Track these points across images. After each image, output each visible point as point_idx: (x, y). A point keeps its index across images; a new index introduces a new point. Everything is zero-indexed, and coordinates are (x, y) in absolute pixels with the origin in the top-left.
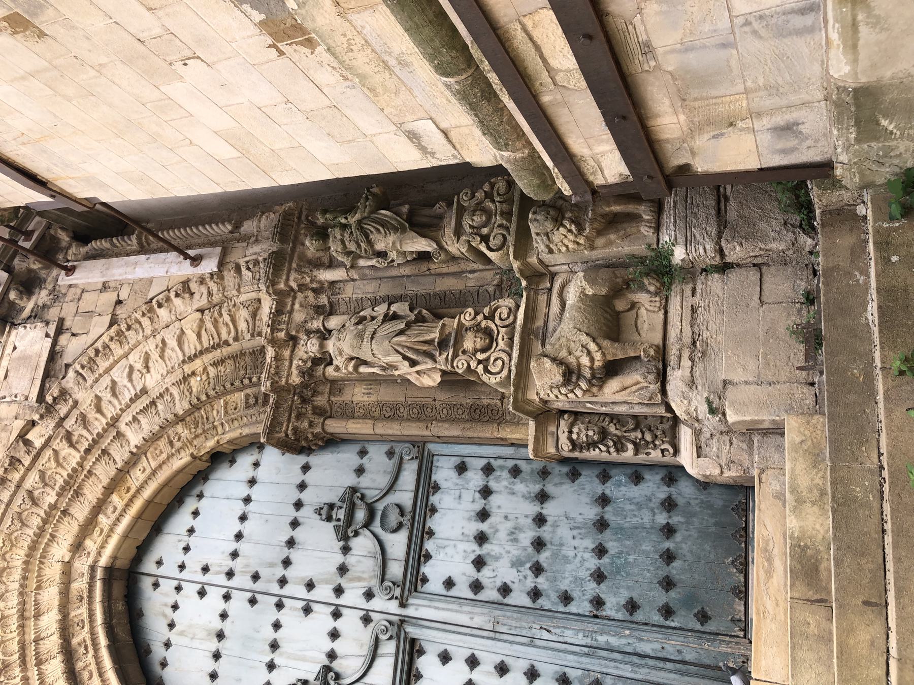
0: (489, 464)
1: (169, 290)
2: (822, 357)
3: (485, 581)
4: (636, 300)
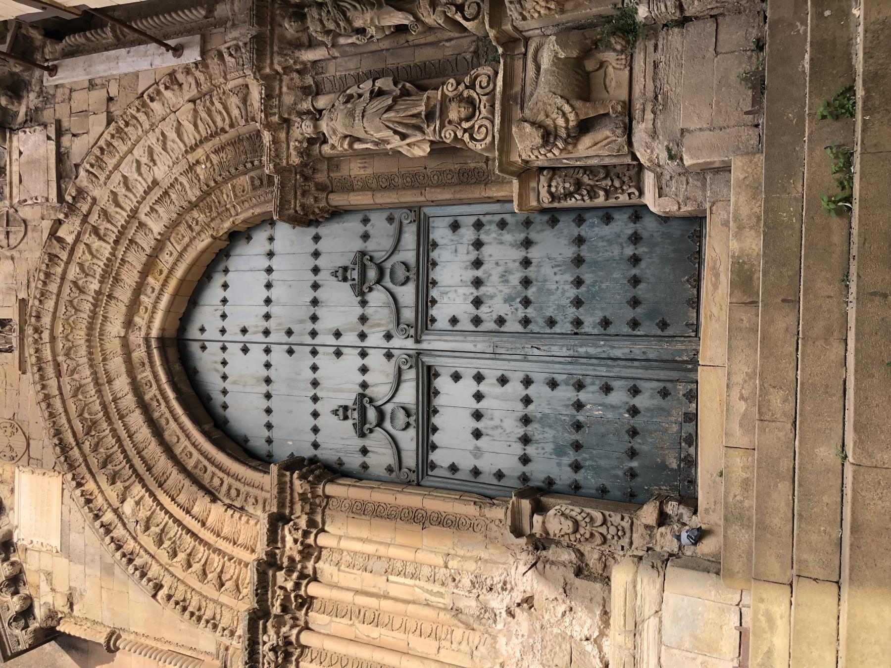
0: (479, 220)
1: (157, 83)
3: (483, 316)
4: (604, 59)
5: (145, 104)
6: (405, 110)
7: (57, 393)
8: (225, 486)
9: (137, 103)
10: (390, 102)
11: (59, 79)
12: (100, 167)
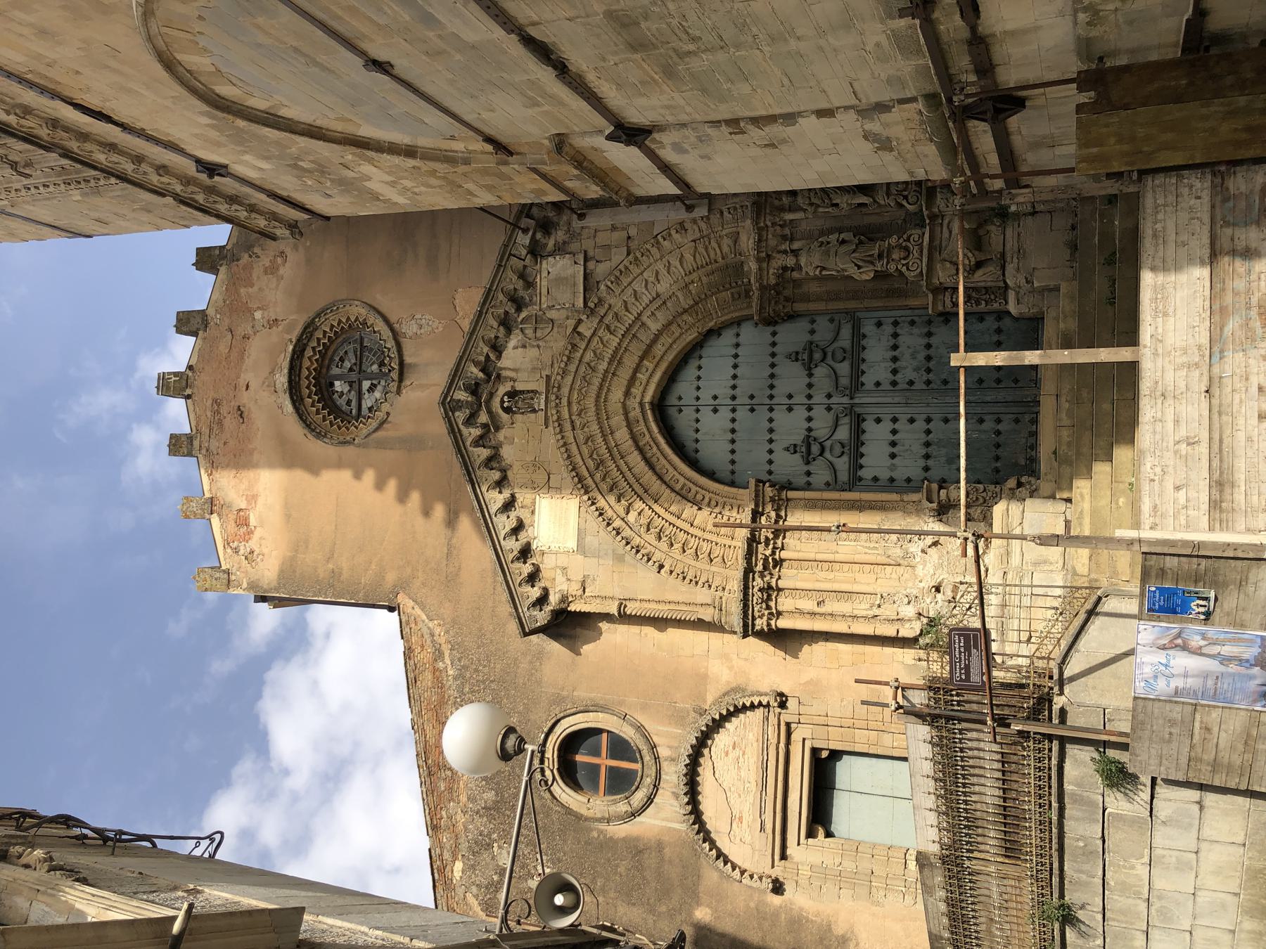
2: (1077, 255)
3: (898, 381)
5: (658, 243)
7: (573, 440)
8: (707, 500)
10: (854, 247)
12: (618, 284)
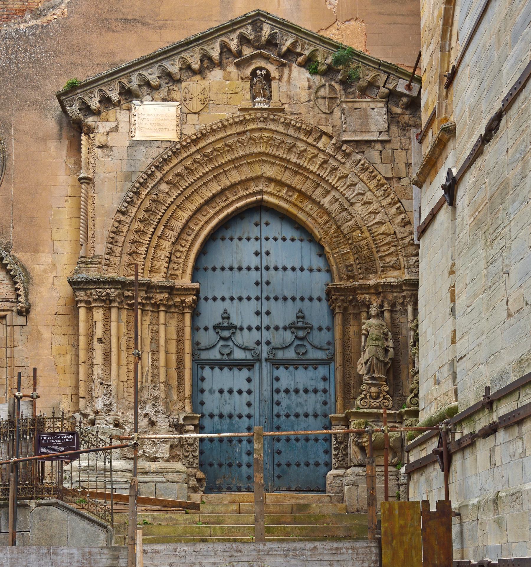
0: (327, 391)
1: (405, 213)
6: (377, 367)
8: (181, 249)
9: (396, 198)
10: (381, 359)
11: (414, 141)
